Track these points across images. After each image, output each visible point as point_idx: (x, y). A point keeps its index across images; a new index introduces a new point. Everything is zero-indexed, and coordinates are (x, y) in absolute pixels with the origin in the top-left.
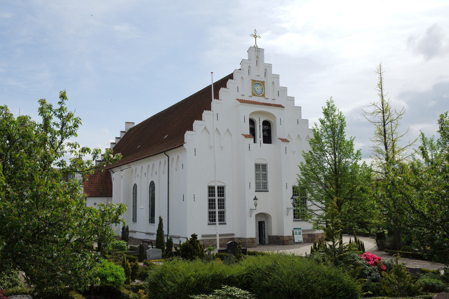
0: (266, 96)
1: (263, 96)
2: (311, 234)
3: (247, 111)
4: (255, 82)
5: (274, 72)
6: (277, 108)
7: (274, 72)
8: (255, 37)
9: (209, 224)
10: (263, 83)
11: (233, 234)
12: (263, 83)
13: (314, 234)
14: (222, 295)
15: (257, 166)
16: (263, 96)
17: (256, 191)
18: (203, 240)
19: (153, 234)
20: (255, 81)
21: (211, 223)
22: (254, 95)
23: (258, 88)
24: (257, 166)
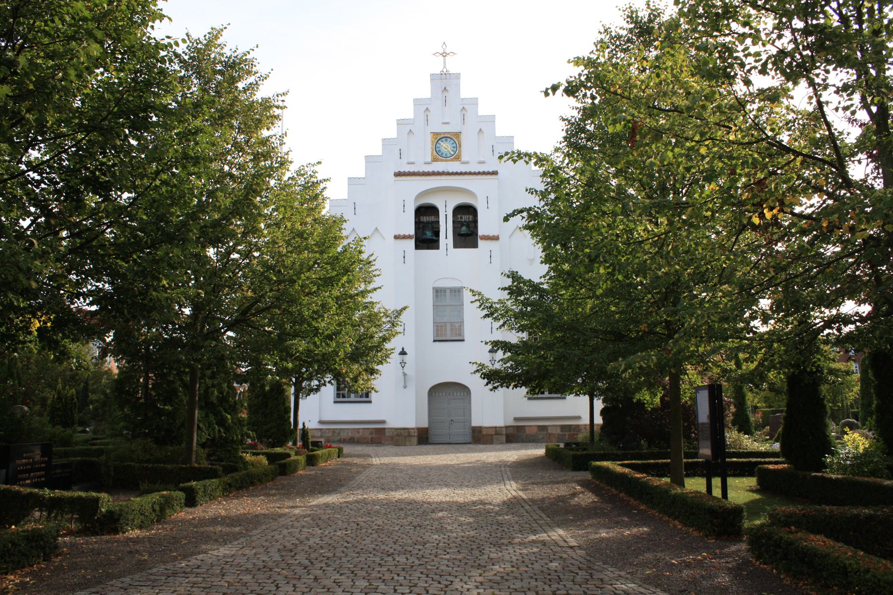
0: (464, 159)
1: (458, 158)
2: (570, 426)
3: (412, 192)
4: (439, 138)
5: (482, 111)
6: (404, 178)
7: (482, 111)
8: (444, 55)
9: (335, 402)
10: (458, 135)
11: (383, 422)
12: (458, 135)
13: (578, 426)
14: (862, 319)
15: (439, 292)
16: (458, 158)
17: (435, 341)
18: (321, 429)
19: (405, 375)
20: (437, 134)
21: (341, 399)
22: (435, 160)
23: (446, 147)
24: (439, 292)
